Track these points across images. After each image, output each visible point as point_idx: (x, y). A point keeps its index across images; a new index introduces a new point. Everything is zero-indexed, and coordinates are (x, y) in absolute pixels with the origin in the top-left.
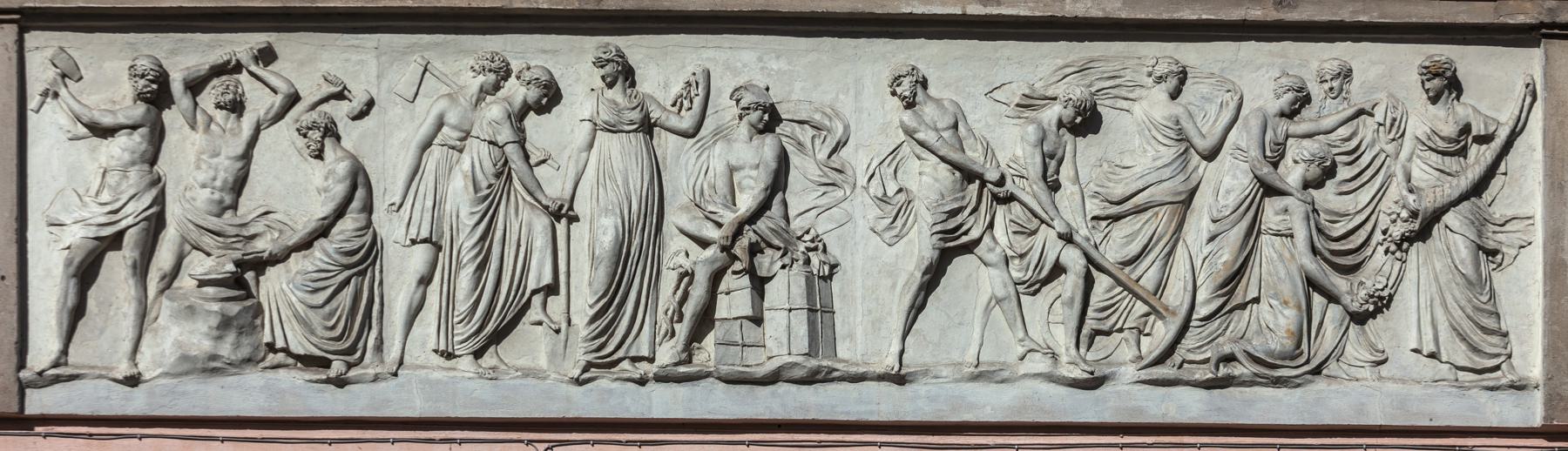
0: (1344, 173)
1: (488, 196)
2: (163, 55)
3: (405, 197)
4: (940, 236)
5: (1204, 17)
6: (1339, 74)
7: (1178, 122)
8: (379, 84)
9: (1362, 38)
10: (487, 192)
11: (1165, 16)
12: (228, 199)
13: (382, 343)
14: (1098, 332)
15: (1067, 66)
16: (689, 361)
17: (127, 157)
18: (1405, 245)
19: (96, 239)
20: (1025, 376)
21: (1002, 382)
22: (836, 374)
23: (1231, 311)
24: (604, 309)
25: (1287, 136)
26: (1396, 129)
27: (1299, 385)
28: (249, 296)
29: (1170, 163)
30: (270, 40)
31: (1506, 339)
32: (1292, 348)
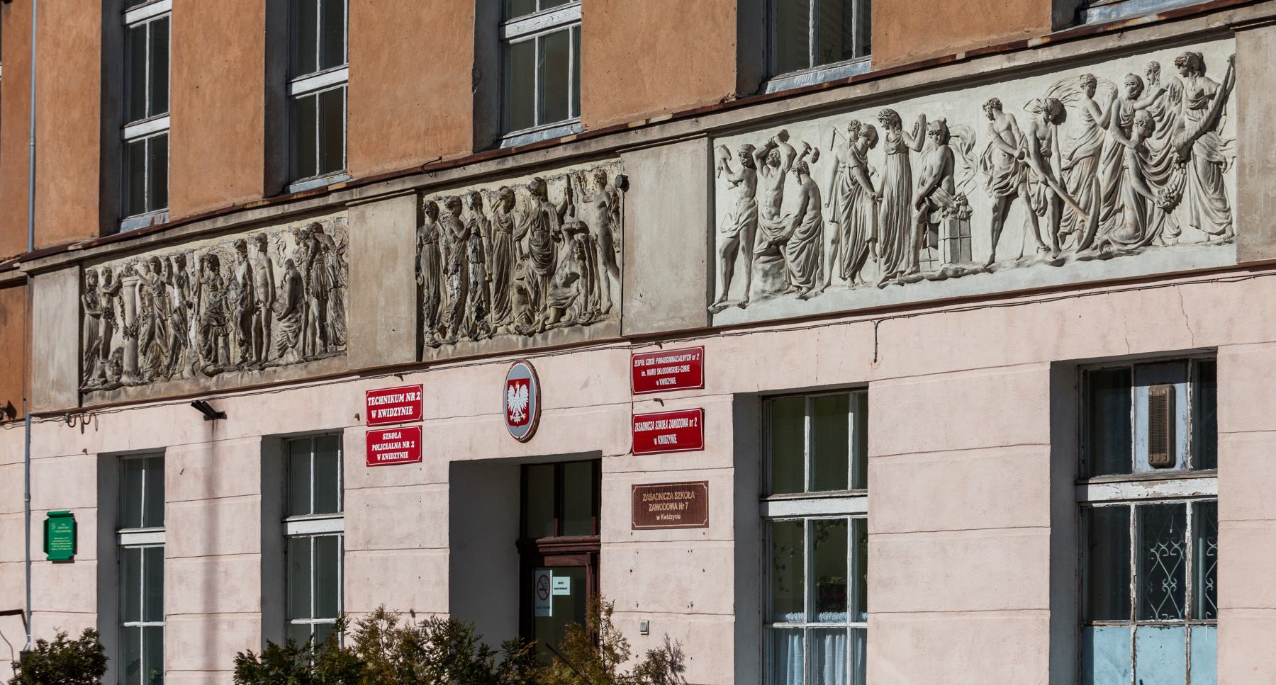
0: (1158, 126)
1: (848, 195)
2: (344, 222)
3: (830, 199)
4: (998, 191)
5: (1091, 51)
6: (1150, 71)
7: (1088, 111)
8: (821, 144)
9: (856, 107)
10: (849, 193)
11: (1076, 54)
12: (773, 211)
13: (823, 275)
14: (1066, 234)
15: (1051, 87)
16: (917, 271)
17: (740, 196)
18: (1182, 165)
19: (731, 237)
20: (1037, 262)
21: (1028, 266)
22: (966, 271)
23: (1115, 214)
24: (108, 331)
25: (1135, 111)
26: (1176, 96)
27: (1139, 253)
28: (782, 258)
29: (1085, 135)
30: (785, 128)
31: (1228, 214)
32: (1132, 232)
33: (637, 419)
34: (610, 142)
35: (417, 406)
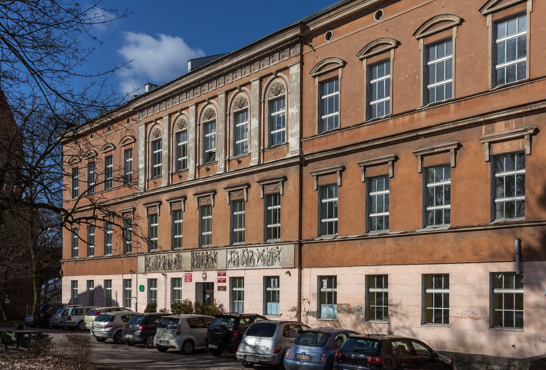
33: (218, 279)
34: (215, 248)
35: (191, 276)
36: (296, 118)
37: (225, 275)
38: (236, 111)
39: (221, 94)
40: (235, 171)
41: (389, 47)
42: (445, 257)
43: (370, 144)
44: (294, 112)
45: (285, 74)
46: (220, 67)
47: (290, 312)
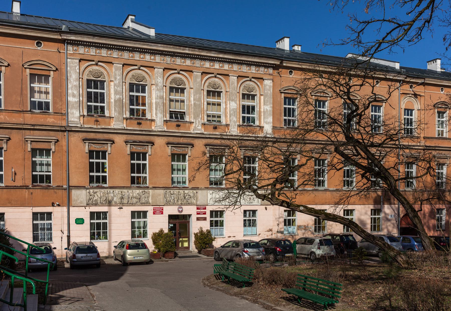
35: (162, 209)
36: (270, 113)
37: (205, 209)
38: (210, 89)
39: (76, 59)
40: (101, 128)
41: (328, 95)
42: (354, 202)
43: (320, 142)
44: (268, 109)
45: (151, 72)
46: (204, 53)
47: (267, 232)
